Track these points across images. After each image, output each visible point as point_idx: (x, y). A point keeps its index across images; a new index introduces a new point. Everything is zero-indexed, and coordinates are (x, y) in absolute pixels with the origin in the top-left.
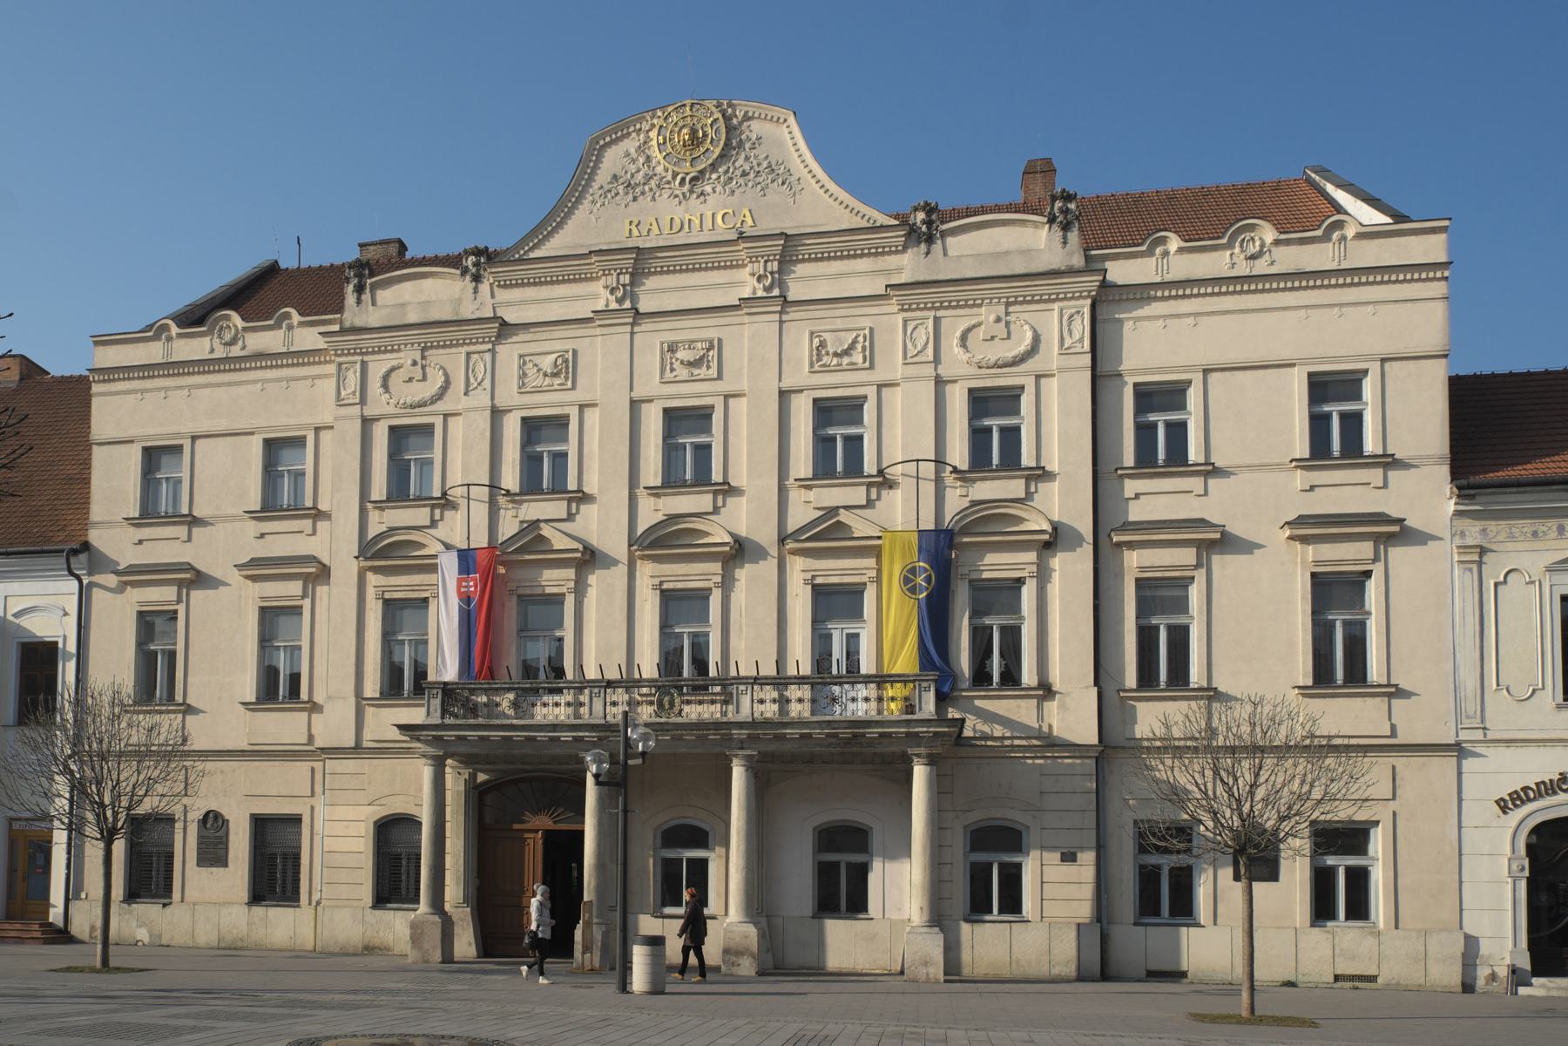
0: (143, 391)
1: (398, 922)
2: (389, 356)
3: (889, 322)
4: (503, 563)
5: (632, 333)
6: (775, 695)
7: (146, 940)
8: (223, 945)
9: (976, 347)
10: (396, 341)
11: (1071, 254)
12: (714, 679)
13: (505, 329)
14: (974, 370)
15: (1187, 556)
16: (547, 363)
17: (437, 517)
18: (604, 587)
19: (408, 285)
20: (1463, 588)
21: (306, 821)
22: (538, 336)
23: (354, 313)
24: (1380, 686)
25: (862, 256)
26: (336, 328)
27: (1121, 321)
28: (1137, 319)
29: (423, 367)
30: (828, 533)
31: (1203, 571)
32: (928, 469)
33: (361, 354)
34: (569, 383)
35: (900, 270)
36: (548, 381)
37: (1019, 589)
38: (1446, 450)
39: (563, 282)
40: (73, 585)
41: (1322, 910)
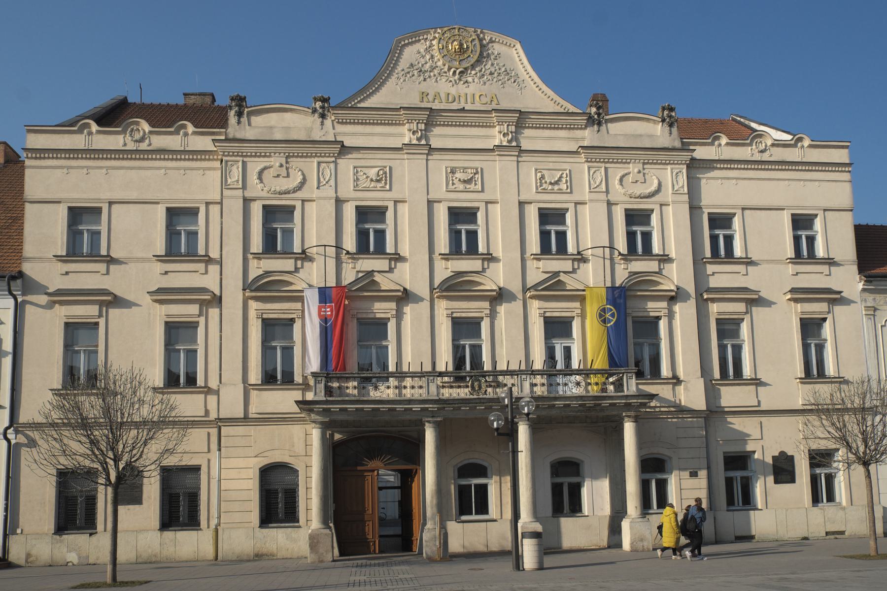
0: (69, 168)
1: (280, 536)
2: (262, 159)
3: (581, 168)
4: (347, 298)
5: (427, 160)
6: (396, 383)
7: (76, 561)
8: (140, 560)
9: (628, 184)
10: (268, 150)
11: (674, 140)
12: (392, 373)
13: (344, 150)
14: (627, 199)
15: (741, 307)
16: (372, 173)
17: (299, 265)
18: (413, 316)
19: (274, 116)
20: (868, 328)
21: (204, 469)
22: (366, 156)
23: (234, 128)
24: (835, 378)
25: (562, 128)
26: (223, 138)
27: (699, 179)
28: (708, 178)
29: (287, 169)
30: (552, 287)
31: (749, 315)
32: (332, 251)
33: (242, 156)
34: (388, 187)
35: (583, 139)
36: (373, 184)
37: (292, 325)
38: (855, 258)
39: (381, 124)
40: (11, 302)
41: (816, 499)
